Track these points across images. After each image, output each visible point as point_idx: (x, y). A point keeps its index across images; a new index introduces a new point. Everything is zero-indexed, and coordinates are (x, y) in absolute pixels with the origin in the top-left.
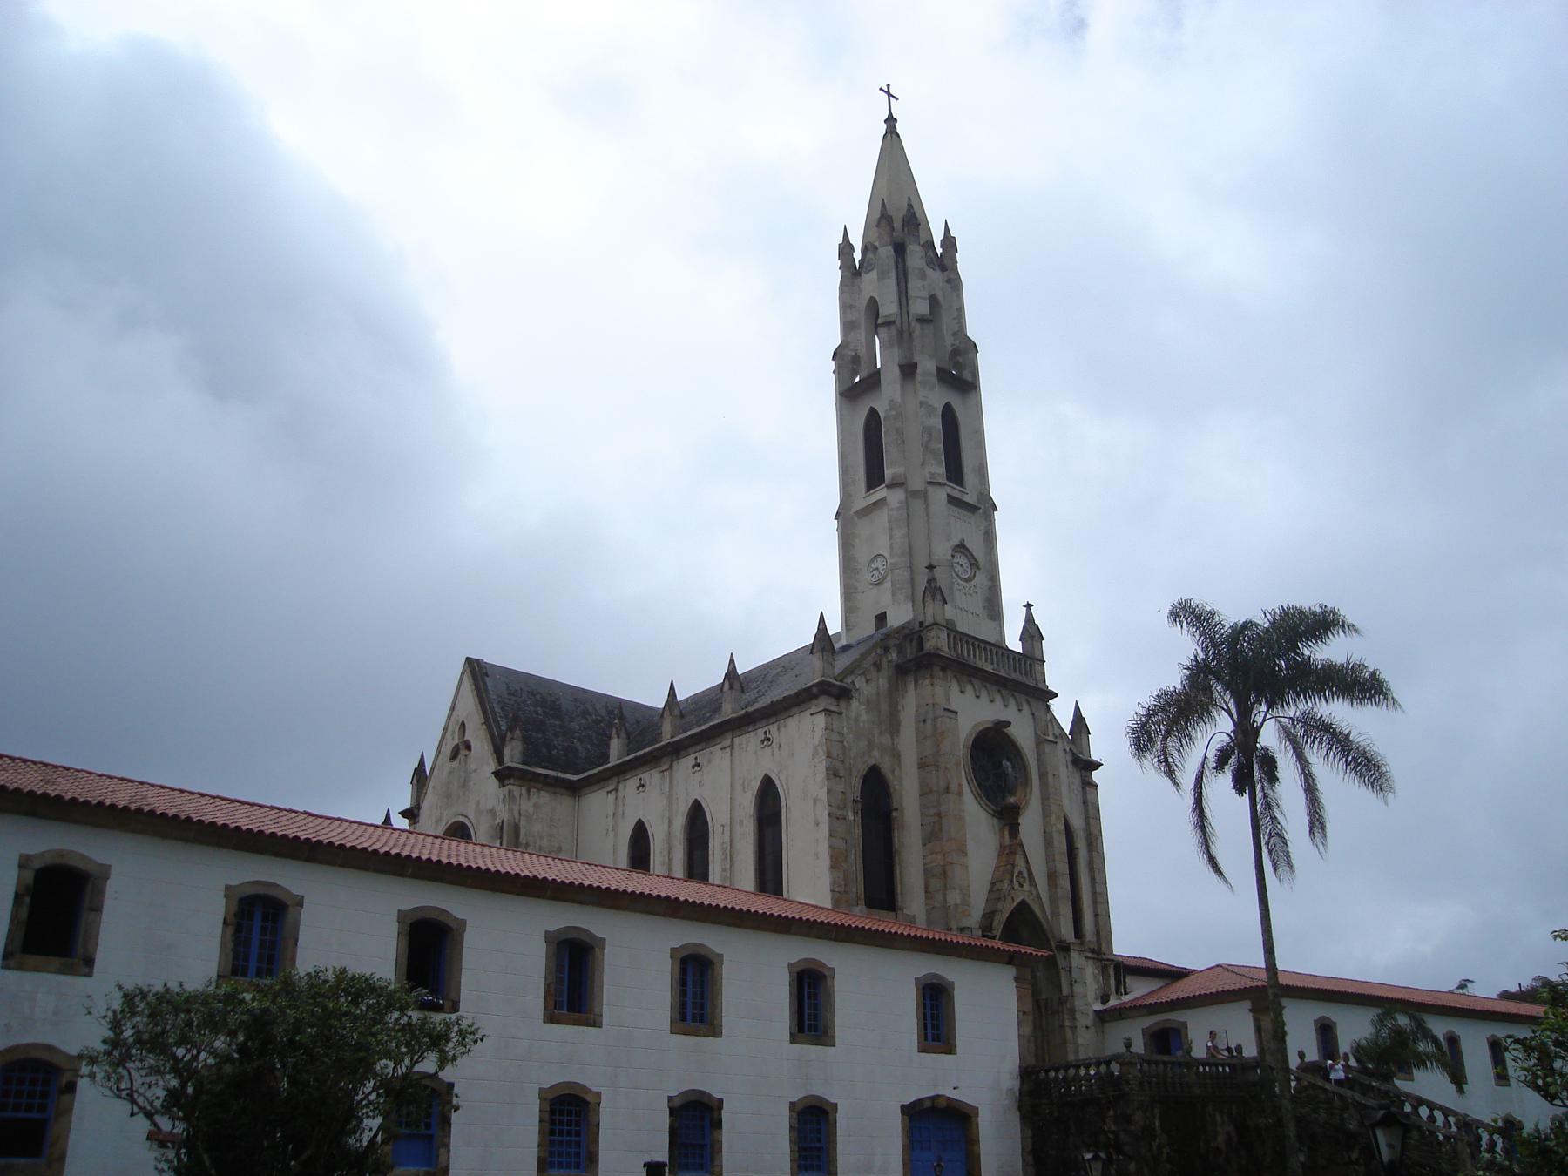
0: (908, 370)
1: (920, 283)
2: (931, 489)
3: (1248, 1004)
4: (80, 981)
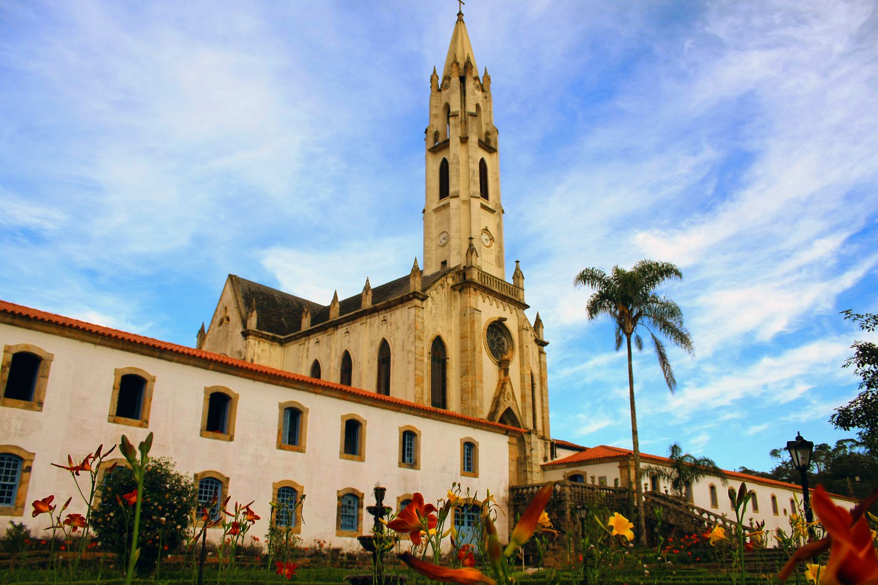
0: (464, 140)
1: (472, 97)
2: (472, 199)
3: (618, 464)
4: (35, 414)
